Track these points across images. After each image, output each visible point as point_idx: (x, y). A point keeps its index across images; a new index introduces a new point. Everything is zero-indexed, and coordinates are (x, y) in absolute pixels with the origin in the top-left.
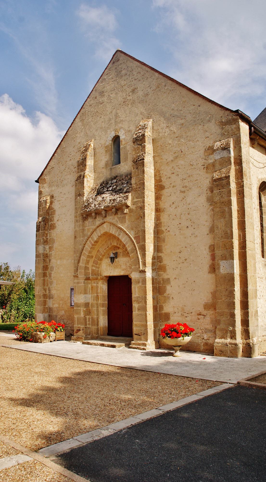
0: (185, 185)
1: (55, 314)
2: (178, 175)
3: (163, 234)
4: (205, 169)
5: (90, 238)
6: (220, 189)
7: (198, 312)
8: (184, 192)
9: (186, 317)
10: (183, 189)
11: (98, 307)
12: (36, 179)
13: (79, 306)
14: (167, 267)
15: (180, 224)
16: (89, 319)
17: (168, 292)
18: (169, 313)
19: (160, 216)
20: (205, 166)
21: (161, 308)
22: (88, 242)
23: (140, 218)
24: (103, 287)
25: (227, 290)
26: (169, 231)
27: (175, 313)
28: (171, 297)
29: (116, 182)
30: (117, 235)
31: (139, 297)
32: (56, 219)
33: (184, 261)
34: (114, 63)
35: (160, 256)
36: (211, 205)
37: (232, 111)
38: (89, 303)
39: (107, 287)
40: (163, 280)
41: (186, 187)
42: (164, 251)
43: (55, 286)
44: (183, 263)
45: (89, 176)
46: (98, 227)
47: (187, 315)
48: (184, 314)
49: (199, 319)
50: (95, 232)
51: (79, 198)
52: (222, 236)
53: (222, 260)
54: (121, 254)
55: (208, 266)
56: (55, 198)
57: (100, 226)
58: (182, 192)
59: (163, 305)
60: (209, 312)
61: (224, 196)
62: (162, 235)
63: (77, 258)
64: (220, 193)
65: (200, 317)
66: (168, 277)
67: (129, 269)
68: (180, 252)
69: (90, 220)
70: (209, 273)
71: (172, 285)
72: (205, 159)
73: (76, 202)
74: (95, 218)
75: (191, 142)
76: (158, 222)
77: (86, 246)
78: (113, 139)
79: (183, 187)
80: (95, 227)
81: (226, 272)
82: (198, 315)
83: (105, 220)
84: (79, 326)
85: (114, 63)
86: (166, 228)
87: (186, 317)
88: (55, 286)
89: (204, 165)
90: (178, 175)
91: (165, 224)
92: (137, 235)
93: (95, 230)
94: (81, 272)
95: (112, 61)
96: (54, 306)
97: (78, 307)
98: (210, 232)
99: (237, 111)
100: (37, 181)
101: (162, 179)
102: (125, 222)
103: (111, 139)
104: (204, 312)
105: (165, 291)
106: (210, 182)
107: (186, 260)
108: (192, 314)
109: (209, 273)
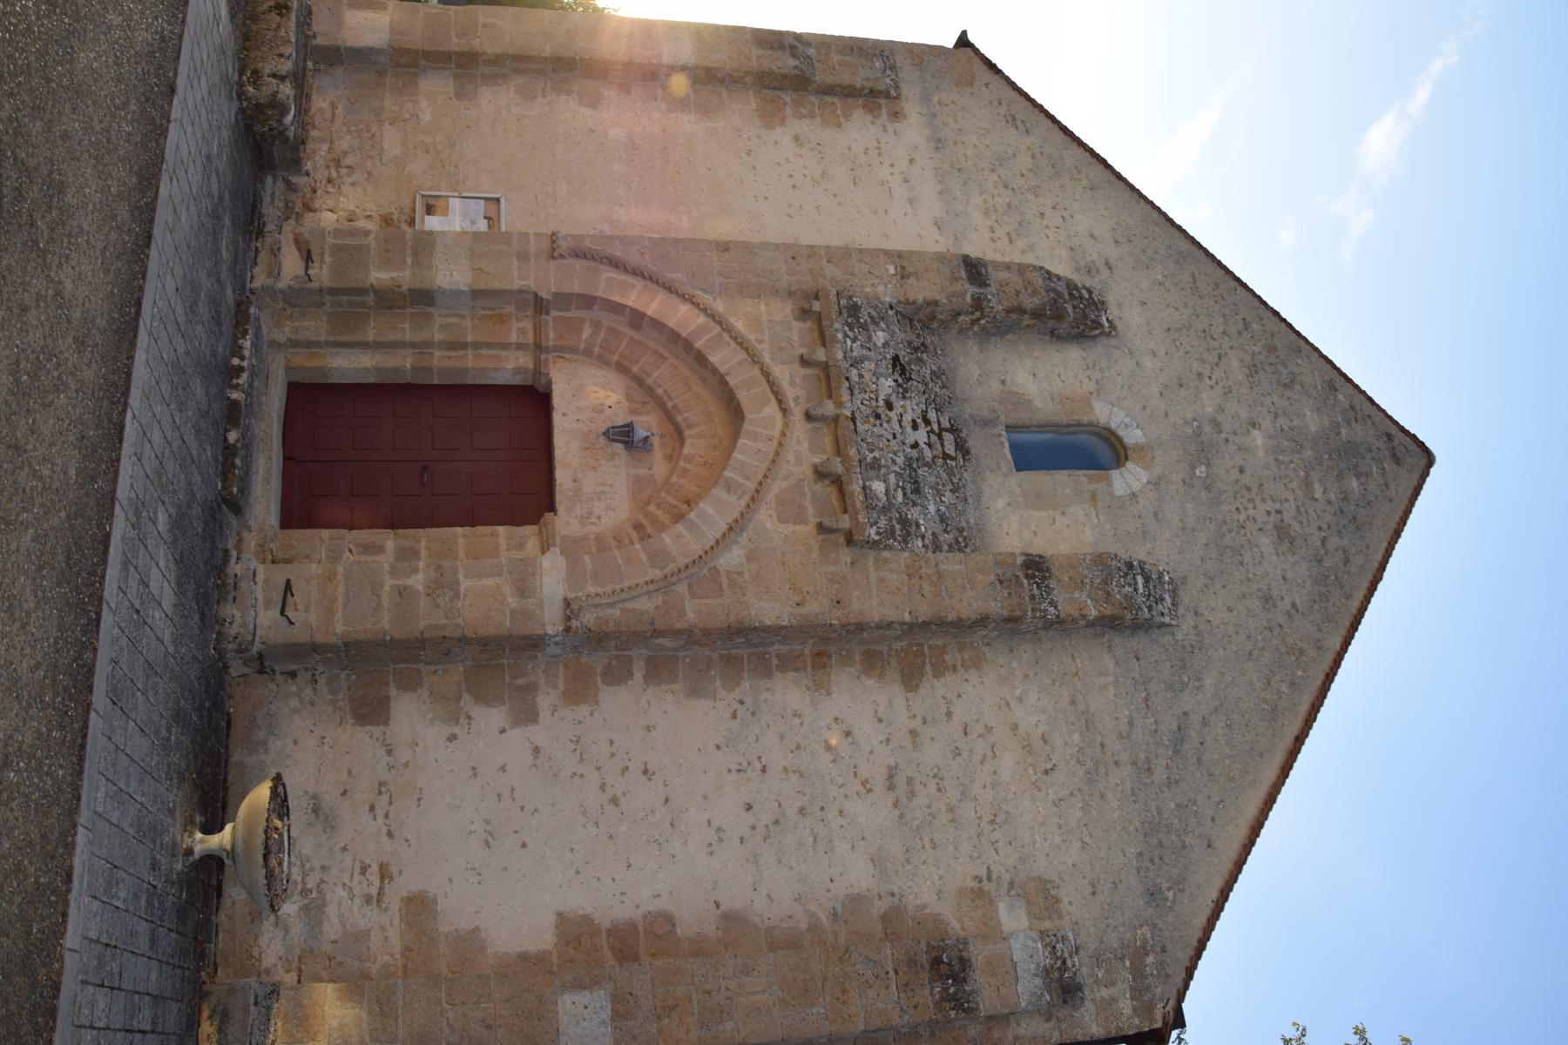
0: (918, 787)
1: (387, 103)
2: (957, 753)
3: (724, 687)
4: (975, 884)
5: (717, 329)
6: (896, 972)
7: (394, 870)
8: (891, 788)
9: (372, 808)
10: (901, 781)
11: (413, 345)
12: (971, 38)
13: (417, 263)
14: (584, 710)
15: (764, 770)
16: (363, 305)
17: (478, 711)
18: (386, 723)
19: (797, 670)
20: (987, 886)
21: (410, 684)
22: (702, 319)
23: (796, 599)
24: (509, 367)
25: (489, 1027)
26: (734, 716)
27: (389, 752)
28: (456, 730)
29: (946, 456)
30: (726, 473)
31: (457, 596)
32: (802, 127)
33: (609, 793)
34: (1389, 437)
35: (630, 675)
36: (835, 914)
37: (1181, 997)
38: (431, 304)
39: (502, 382)
40: (532, 689)
41: (912, 794)
42: (651, 691)
43: (515, 110)
44: (603, 788)
45: (978, 320)
46: (767, 374)
47: (380, 812)
48: (385, 798)
49: (364, 870)
50: (744, 356)
51: (892, 270)
52: (709, 992)
53: (615, 999)
54: (642, 472)
55: (589, 910)
56: (890, 127)
57: (771, 384)
58: (891, 777)
59: (424, 691)
60: (396, 922)
61: (871, 993)
62: (718, 683)
63: (633, 258)
64: (882, 974)
65: (374, 875)
66: (544, 715)
67: (578, 511)
68: (645, 772)
69: (798, 334)
70: (559, 914)
71: (509, 733)
72: (1012, 884)
73: (875, 253)
74: (805, 362)
75: (1079, 814)
76: (775, 661)
77: (685, 308)
78: (1113, 433)
79: (910, 780)
80: (767, 359)
81: (563, 1018)
82: (381, 866)
83: (800, 428)
84: (328, 259)
85: (1389, 437)
86: (748, 700)
87: (372, 808)
88: (515, 110)
89: (989, 879)
90: (957, 753)
91: (765, 695)
92: (725, 582)
93: (754, 359)
94: (575, 277)
95: (1393, 430)
96: (424, 103)
97: (415, 255)
98: (726, 916)
99: (1179, 1022)
100: (963, 41)
101: (949, 678)
102: (782, 520)
103: (1113, 426)
104: (393, 899)
105: (483, 698)
106: (925, 907)
107: (615, 801)
108: (385, 839)
109: (559, 914)
